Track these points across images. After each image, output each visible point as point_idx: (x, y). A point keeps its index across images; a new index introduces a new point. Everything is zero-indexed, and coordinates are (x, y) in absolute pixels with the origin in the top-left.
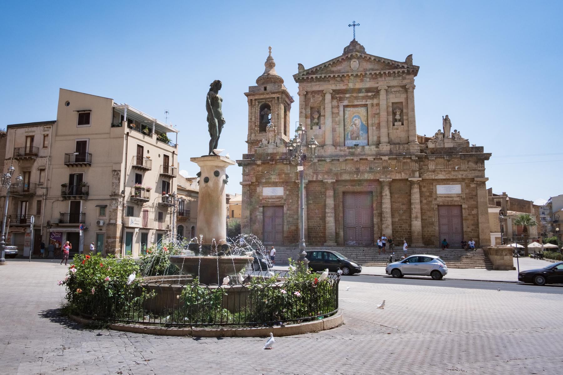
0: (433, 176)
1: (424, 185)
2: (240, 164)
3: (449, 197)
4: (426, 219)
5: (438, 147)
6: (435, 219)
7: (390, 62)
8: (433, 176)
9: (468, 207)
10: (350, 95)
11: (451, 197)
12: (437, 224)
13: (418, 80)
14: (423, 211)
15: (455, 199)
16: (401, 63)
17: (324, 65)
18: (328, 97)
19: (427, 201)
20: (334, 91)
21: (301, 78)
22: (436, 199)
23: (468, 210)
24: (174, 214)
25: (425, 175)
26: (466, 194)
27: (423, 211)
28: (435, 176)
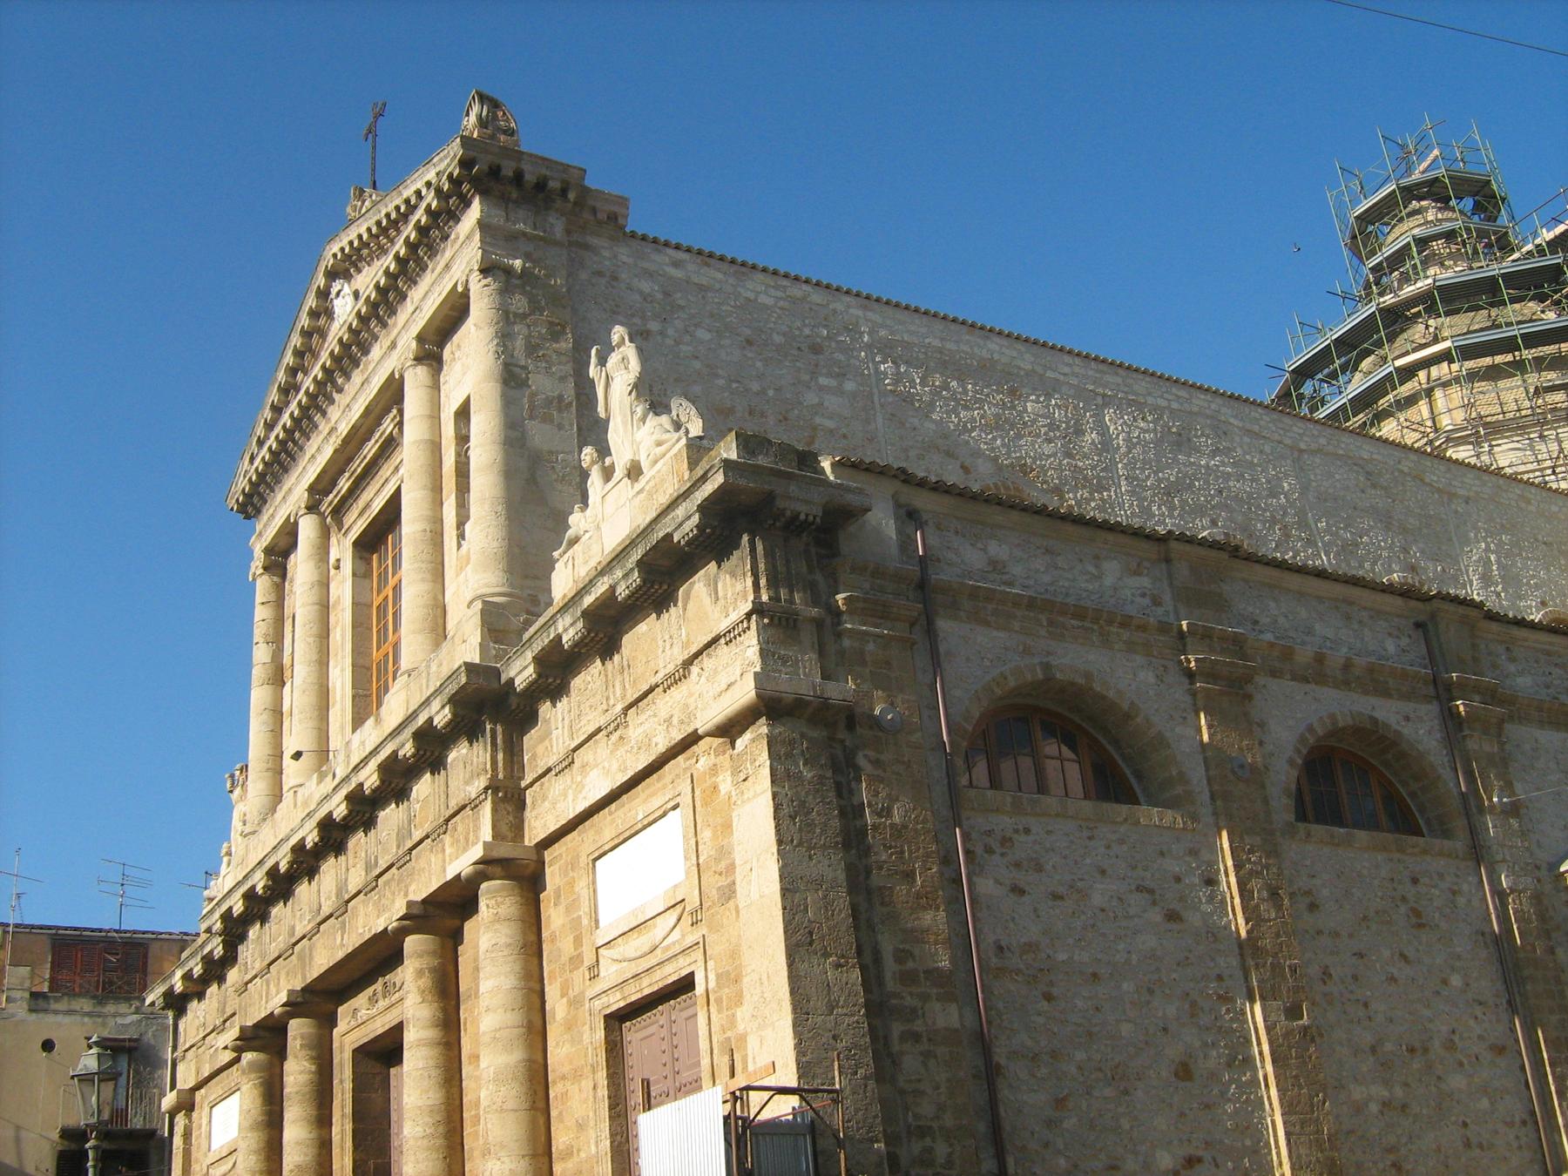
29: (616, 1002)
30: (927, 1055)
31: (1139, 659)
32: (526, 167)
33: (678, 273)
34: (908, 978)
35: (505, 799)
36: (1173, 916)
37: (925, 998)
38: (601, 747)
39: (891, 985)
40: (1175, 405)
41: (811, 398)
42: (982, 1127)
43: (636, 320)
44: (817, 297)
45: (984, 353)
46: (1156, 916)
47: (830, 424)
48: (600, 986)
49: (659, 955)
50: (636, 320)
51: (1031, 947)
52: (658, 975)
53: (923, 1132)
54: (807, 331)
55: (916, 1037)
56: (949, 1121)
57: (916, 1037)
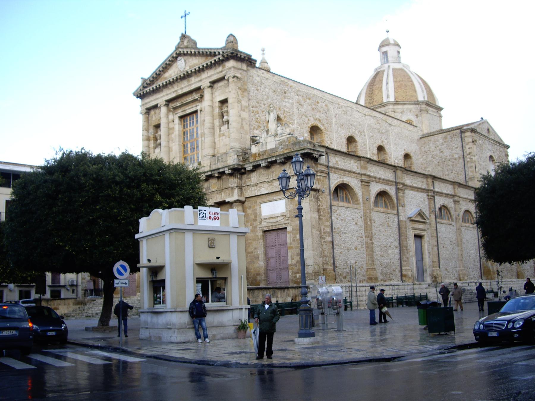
0: (256, 191)
1: (250, 205)
2: (165, 105)
3: (273, 218)
4: (252, 252)
5: (261, 150)
6: (260, 251)
7: (207, 51)
8: (256, 191)
9: (293, 229)
10: (113, 315)
11: (275, 217)
12: (262, 257)
13: (442, 118)
14: (249, 241)
15: (279, 219)
16: (221, 49)
17: (155, 74)
18: (164, 110)
19: (252, 227)
20: (167, 101)
21: (201, 53)
22: (260, 223)
23: (293, 233)
24: (174, 92)
25: (249, 191)
26: (290, 211)
27: (249, 241)
28: (258, 191)
29: (266, 229)
30: (326, 245)
31: (355, 179)
32: (242, 54)
33: (263, 75)
34: (324, 233)
35: (239, 188)
36: (356, 224)
37: (326, 236)
38: (266, 185)
39: (322, 234)
40: (345, 105)
41: (284, 104)
42: (332, 256)
43: (256, 87)
44: (286, 81)
45: (313, 93)
46: (354, 223)
47: (287, 110)
48: (261, 226)
49: (278, 223)
50: (256, 87)
51: (338, 228)
52: (277, 226)
53: (325, 256)
54: (284, 88)
55: (325, 242)
56: (328, 255)
57: (325, 242)
